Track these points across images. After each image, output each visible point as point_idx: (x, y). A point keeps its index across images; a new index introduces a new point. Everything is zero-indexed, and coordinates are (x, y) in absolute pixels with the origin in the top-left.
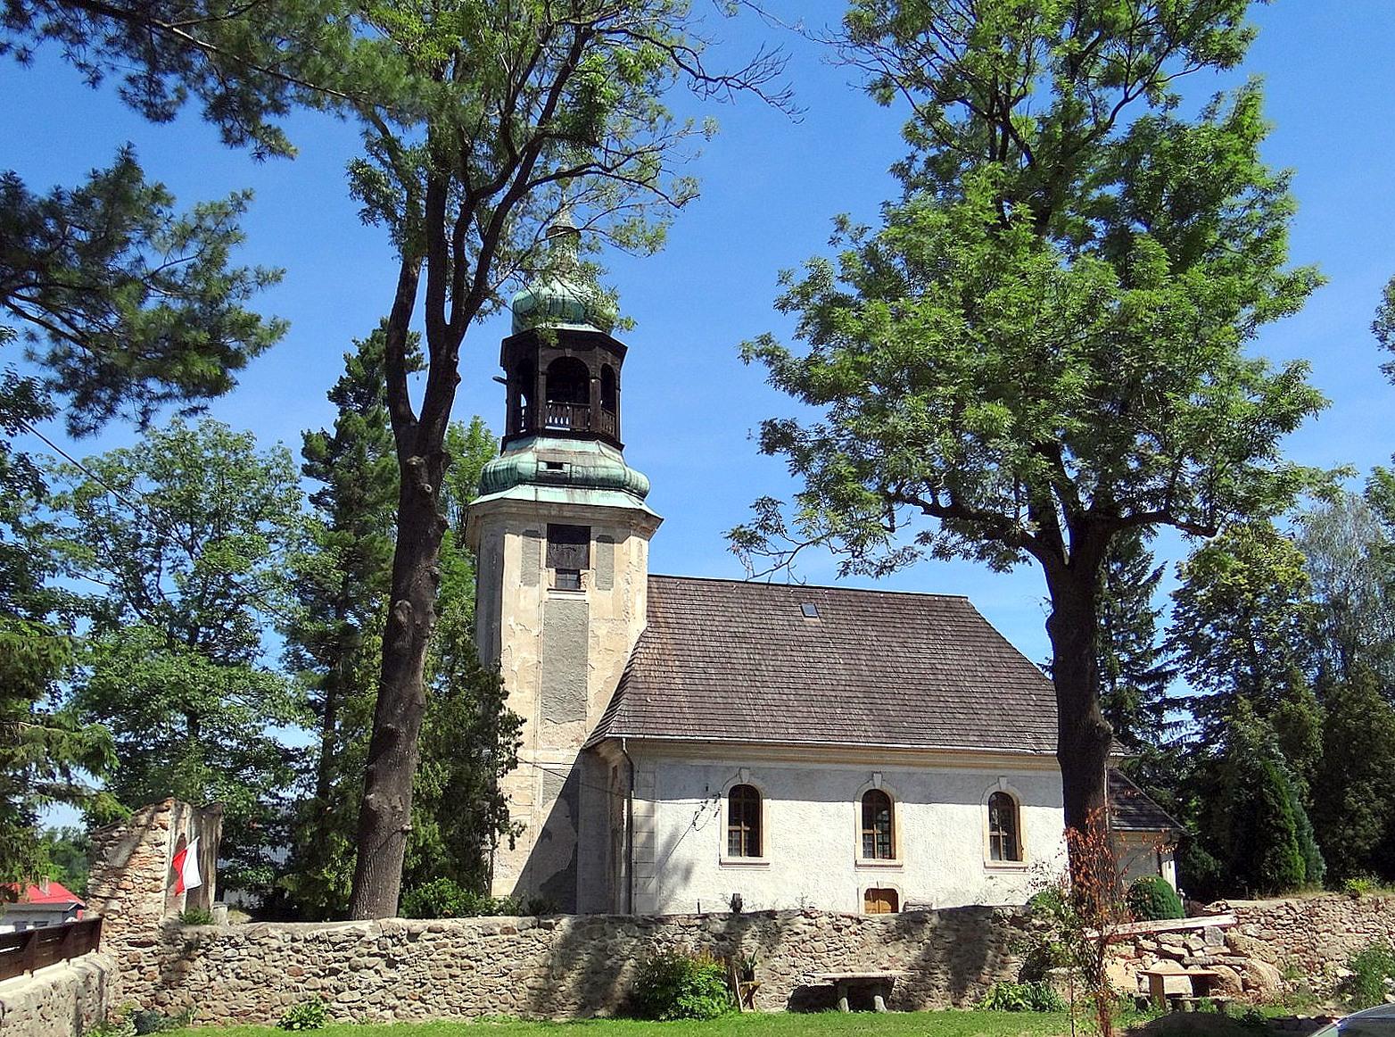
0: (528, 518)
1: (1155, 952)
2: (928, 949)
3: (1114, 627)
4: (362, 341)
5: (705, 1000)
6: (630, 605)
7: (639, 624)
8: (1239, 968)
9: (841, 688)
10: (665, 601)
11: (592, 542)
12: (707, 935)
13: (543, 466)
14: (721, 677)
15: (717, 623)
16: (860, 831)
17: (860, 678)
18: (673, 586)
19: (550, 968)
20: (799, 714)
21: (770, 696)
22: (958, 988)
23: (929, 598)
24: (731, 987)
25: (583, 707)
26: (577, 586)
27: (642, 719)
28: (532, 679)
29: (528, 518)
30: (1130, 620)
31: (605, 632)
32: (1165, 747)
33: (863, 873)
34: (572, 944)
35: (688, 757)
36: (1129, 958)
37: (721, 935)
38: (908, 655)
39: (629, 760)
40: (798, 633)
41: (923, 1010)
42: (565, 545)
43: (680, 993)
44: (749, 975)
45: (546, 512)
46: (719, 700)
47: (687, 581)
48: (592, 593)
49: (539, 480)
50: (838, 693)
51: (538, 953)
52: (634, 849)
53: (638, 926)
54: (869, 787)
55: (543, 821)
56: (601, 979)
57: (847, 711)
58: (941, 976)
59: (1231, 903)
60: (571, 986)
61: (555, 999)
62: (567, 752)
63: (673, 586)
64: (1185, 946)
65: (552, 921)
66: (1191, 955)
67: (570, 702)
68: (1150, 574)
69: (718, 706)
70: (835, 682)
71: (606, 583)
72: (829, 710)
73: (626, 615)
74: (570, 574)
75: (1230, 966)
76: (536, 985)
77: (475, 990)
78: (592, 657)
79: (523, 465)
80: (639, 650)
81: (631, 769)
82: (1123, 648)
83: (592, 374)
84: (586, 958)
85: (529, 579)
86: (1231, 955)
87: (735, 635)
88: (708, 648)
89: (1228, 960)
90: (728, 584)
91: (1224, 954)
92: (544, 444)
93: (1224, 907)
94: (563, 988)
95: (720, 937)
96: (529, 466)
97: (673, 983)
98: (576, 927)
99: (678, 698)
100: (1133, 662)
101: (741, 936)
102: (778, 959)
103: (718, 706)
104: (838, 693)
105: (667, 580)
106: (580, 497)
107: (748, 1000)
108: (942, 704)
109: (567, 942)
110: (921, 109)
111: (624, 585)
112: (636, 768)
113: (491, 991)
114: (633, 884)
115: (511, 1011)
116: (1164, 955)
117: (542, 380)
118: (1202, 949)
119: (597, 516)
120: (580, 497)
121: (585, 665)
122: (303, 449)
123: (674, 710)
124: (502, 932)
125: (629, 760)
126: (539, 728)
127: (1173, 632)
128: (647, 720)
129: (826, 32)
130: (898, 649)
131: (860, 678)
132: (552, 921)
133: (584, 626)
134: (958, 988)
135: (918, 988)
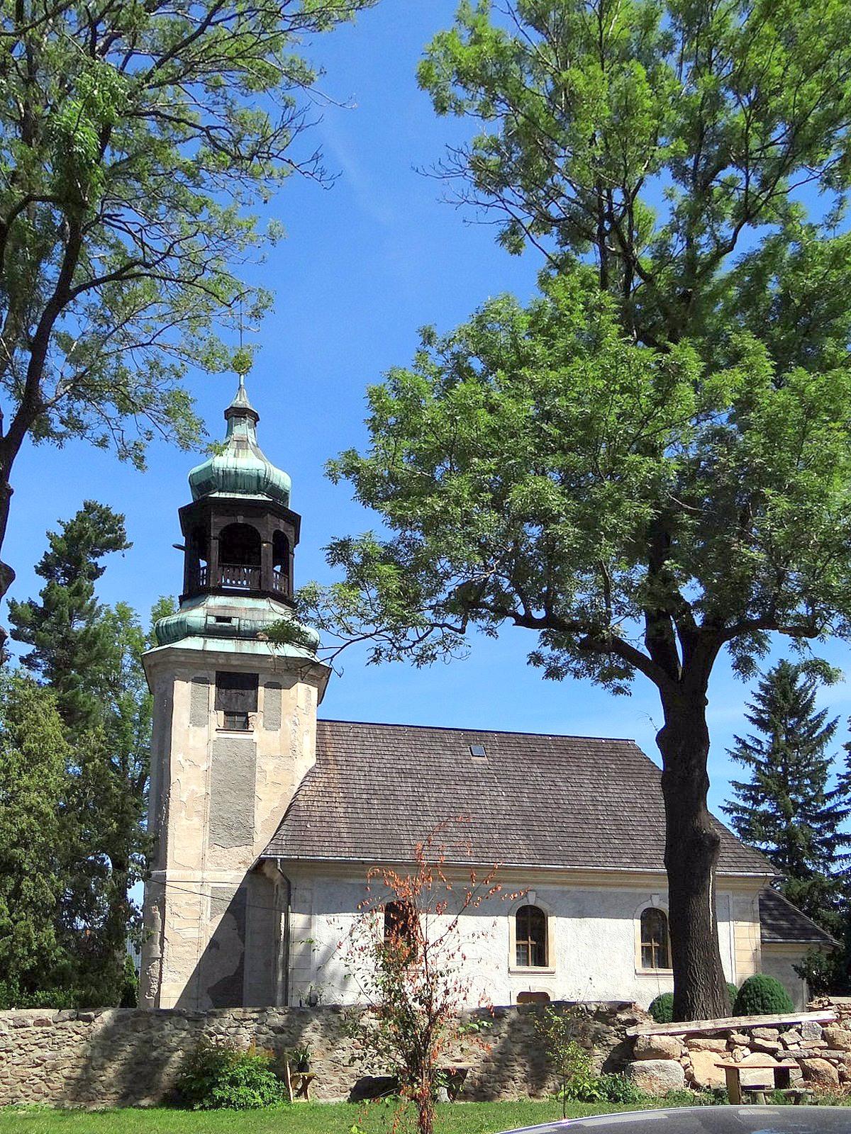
0: (197, 667)
1: (747, 1046)
2: (504, 1043)
3: (791, 773)
4: (67, 521)
5: (243, 1090)
6: (297, 743)
7: (307, 759)
8: (836, 1061)
9: (500, 817)
10: (337, 742)
11: (260, 688)
12: (265, 1029)
13: (212, 620)
14: (383, 806)
15: (385, 761)
16: (514, 942)
17: (521, 808)
18: (347, 729)
19: (90, 1059)
20: (455, 839)
21: (429, 824)
22: (537, 1079)
23: (597, 741)
24: (281, 1077)
25: (250, 833)
26: (245, 727)
27: (299, 842)
28: (200, 808)
29: (197, 667)
30: (805, 767)
31: (272, 768)
32: (835, 876)
33: (516, 978)
34: (113, 1036)
35: (346, 876)
36: (720, 1051)
37: (279, 1028)
38: (570, 789)
39: (286, 878)
40: (463, 770)
41: (498, 1101)
42: (234, 691)
43: (216, 1084)
44: (303, 1066)
45: (214, 661)
46: (379, 827)
47: (360, 726)
48: (259, 732)
49: (209, 632)
50: (497, 822)
51: (75, 1044)
52: (291, 957)
53: (188, 1019)
54: (524, 903)
55: (211, 933)
56: (148, 1069)
57: (504, 837)
58: (518, 1068)
59: (833, 1000)
60: (112, 1076)
61: (94, 1089)
62: (235, 873)
63: (347, 729)
64: (779, 1040)
65: (92, 1014)
66: (786, 1048)
67: (237, 829)
68: (824, 727)
69: (376, 832)
70: (495, 812)
71: (274, 723)
72: (486, 836)
73: (293, 752)
74: (238, 717)
75: (827, 1059)
76: (74, 1075)
77: (5, 1080)
78: (260, 790)
79: (192, 619)
80: (305, 783)
81: (288, 886)
82: (798, 790)
83: (263, 538)
84: (129, 1049)
85: (197, 721)
86: (827, 1048)
87: (400, 772)
88: (373, 783)
89: (825, 1053)
90: (401, 728)
91: (821, 1048)
92: (215, 602)
93: (826, 1003)
94: (103, 1078)
95: (279, 1030)
96: (198, 620)
97: (209, 1073)
98: (118, 1020)
99: (338, 825)
100: (807, 803)
101: (301, 1029)
102: (341, 1051)
103: (376, 832)
104: (497, 822)
105: (341, 724)
106: (247, 647)
107: (302, 1092)
108: (599, 831)
109: (108, 1033)
110: (554, 258)
111: (290, 726)
112: (293, 885)
113: (23, 1081)
114: (290, 987)
115: (45, 1100)
116: (755, 1048)
117: (215, 544)
118: (798, 1043)
119: (264, 665)
120: (247, 647)
121: (251, 795)
122: (10, 616)
123: (333, 835)
124: (36, 1024)
125: (286, 878)
126: (207, 852)
127: (844, 777)
128: (305, 843)
129: (438, 167)
130: (561, 784)
131: (521, 808)
132: (92, 1014)
133: (252, 764)
134: (537, 1079)
135: (492, 1080)
